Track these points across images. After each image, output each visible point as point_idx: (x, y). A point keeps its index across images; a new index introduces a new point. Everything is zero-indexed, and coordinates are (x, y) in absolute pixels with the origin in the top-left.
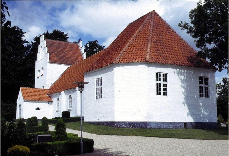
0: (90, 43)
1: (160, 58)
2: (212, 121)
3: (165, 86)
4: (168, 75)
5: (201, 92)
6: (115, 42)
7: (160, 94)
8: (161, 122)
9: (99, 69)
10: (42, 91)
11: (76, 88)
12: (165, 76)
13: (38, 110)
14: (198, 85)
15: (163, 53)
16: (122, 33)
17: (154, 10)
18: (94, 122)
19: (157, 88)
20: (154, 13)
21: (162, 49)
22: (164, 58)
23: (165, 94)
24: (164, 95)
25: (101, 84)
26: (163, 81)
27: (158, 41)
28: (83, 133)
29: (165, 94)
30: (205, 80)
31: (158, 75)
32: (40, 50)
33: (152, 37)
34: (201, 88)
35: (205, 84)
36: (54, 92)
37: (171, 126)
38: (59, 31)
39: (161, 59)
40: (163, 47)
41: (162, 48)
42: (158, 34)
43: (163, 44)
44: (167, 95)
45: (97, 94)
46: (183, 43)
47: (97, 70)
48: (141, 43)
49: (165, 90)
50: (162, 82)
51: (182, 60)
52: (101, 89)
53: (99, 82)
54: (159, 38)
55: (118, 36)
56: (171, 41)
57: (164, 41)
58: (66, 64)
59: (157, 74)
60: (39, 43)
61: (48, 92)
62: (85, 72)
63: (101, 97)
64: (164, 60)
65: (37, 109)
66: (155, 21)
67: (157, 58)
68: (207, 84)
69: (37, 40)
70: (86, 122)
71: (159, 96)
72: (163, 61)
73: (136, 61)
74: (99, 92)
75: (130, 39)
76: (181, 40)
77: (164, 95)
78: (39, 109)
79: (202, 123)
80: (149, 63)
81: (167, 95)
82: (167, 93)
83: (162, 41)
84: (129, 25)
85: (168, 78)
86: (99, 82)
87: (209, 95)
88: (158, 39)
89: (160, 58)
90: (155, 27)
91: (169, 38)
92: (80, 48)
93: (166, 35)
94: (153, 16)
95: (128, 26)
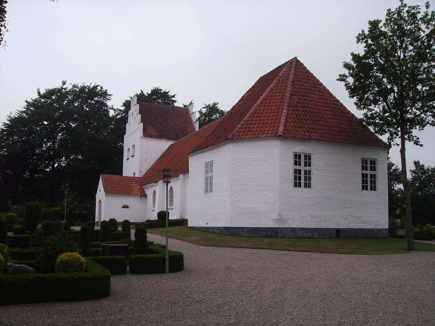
0: (208, 107)
1: (300, 131)
2: (379, 227)
3: (308, 173)
4: (312, 157)
5: (364, 182)
6: (237, 105)
7: (300, 186)
8: (299, 228)
9: (214, 146)
10: (133, 179)
11: (178, 176)
12: (308, 157)
13: (125, 209)
14: (359, 172)
15: (306, 123)
16: (248, 92)
17: (296, 57)
18: (201, 228)
19: (363, 181)
20: (295, 61)
21: (305, 117)
22: (307, 131)
23: (308, 185)
24: (305, 186)
25: (211, 171)
26: (305, 166)
27: (299, 105)
28: (169, 241)
29: (308, 185)
30: (371, 164)
31: (297, 156)
32: (131, 119)
33: (290, 99)
34: (364, 176)
35: (371, 170)
36: (149, 182)
37: (315, 234)
38: (161, 90)
39: (303, 133)
40: (307, 114)
41: (306, 115)
42: (300, 93)
43: (308, 109)
44: (375, 190)
45: (207, 185)
46: (339, 107)
47: (206, 149)
48: (273, 108)
49: (308, 179)
50: (302, 168)
51: (335, 133)
52: (211, 178)
53: (209, 166)
54: (301, 99)
55: (242, 98)
56: (320, 104)
57: (310, 104)
58: (169, 138)
59: (296, 155)
60: (130, 109)
61: (141, 181)
62: (190, 153)
63: (211, 191)
64: (307, 133)
65: (124, 207)
66: (296, 73)
67: (297, 131)
68: (375, 170)
69: (127, 105)
70: (190, 227)
71: (297, 189)
72: (306, 135)
73: (264, 136)
74: (209, 182)
75: (257, 102)
76: (336, 103)
77: (305, 186)
78: (127, 207)
79: (364, 229)
80: (283, 137)
81: (375, 190)
82: (375, 187)
83: (306, 105)
84: (260, 79)
85: (313, 161)
86: (209, 166)
87: (376, 188)
88: (301, 101)
89: (300, 131)
90: (295, 83)
91: (318, 100)
92: (191, 114)
93: (313, 95)
94: (293, 66)
95: (257, 82)
